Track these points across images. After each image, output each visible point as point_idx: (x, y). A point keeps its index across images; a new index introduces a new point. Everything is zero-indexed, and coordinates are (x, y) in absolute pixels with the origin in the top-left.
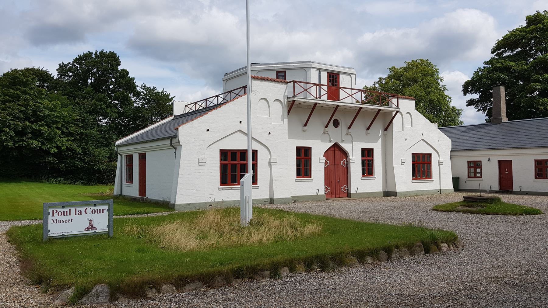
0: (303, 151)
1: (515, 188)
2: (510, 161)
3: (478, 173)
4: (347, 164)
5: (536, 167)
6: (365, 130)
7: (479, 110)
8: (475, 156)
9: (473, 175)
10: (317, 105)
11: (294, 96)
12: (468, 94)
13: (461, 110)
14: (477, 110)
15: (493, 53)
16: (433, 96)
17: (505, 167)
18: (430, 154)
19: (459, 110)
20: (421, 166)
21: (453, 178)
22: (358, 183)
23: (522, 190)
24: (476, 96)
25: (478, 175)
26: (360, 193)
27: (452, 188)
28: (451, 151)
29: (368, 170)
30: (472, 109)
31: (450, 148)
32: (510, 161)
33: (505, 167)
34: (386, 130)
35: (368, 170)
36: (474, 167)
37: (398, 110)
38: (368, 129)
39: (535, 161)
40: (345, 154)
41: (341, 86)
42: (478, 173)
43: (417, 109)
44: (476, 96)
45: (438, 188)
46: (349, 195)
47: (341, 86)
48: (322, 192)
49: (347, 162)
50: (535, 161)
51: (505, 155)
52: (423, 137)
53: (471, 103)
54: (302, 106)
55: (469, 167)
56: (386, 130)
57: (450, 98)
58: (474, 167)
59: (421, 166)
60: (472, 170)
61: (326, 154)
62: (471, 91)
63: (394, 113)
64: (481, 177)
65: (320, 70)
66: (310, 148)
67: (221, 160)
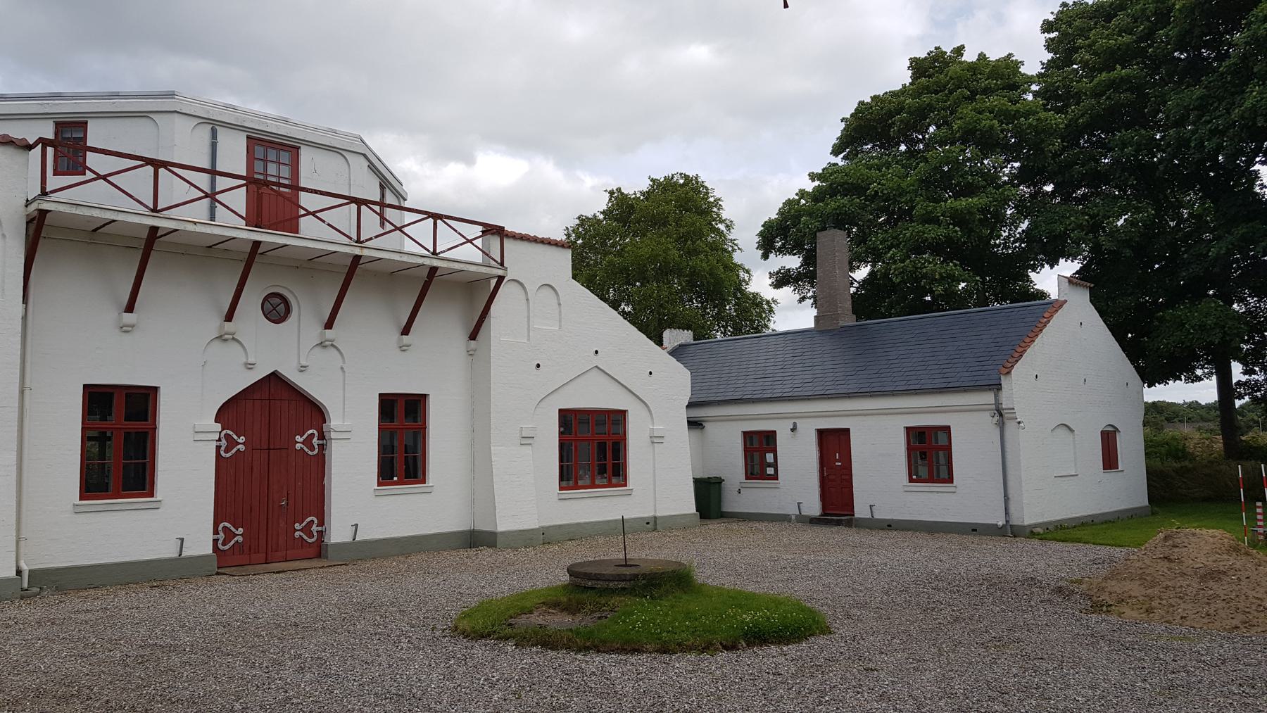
0: (399, 410)
1: (861, 511)
2: (846, 432)
3: (770, 465)
4: (322, 447)
5: (910, 449)
6: (396, 335)
7: (802, 299)
8: (761, 418)
9: (757, 469)
10: (48, 215)
11: (44, 193)
12: (772, 256)
13: (774, 301)
14: (798, 297)
15: (836, 152)
16: (700, 262)
17: (834, 445)
18: (623, 413)
19: (768, 302)
20: (592, 446)
21: (698, 482)
22: (357, 503)
23: (876, 516)
24: (793, 262)
25: (770, 471)
26: (191, 558)
27: (693, 510)
28: (690, 405)
29: (402, 459)
30: (786, 294)
31: (686, 396)
32: (846, 432)
33: (834, 445)
34: (473, 336)
35: (402, 459)
36: (760, 448)
37: (500, 272)
38: (406, 331)
39: (909, 430)
40: (315, 413)
41: (302, 185)
42: (770, 465)
43: (574, 277)
44: (793, 262)
45: (651, 514)
46: (318, 550)
47: (568, 254)
48: (201, 543)
49: (322, 437)
50: (909, 430)
51: (833, 414)
52: (597, 361)
53: (782, 279)
54: (96, 237)
55: (748, 451)
56: (473, 336)
57: (748, 271)
58: (760, 448)
59: (592, 446)
60: (756, 456)
61: (229, 413)
62: (781, 251)
63: (494, 282)
64: (775, 477)
65: (214, 126)
66: (424, 397)
67: (561, 433)
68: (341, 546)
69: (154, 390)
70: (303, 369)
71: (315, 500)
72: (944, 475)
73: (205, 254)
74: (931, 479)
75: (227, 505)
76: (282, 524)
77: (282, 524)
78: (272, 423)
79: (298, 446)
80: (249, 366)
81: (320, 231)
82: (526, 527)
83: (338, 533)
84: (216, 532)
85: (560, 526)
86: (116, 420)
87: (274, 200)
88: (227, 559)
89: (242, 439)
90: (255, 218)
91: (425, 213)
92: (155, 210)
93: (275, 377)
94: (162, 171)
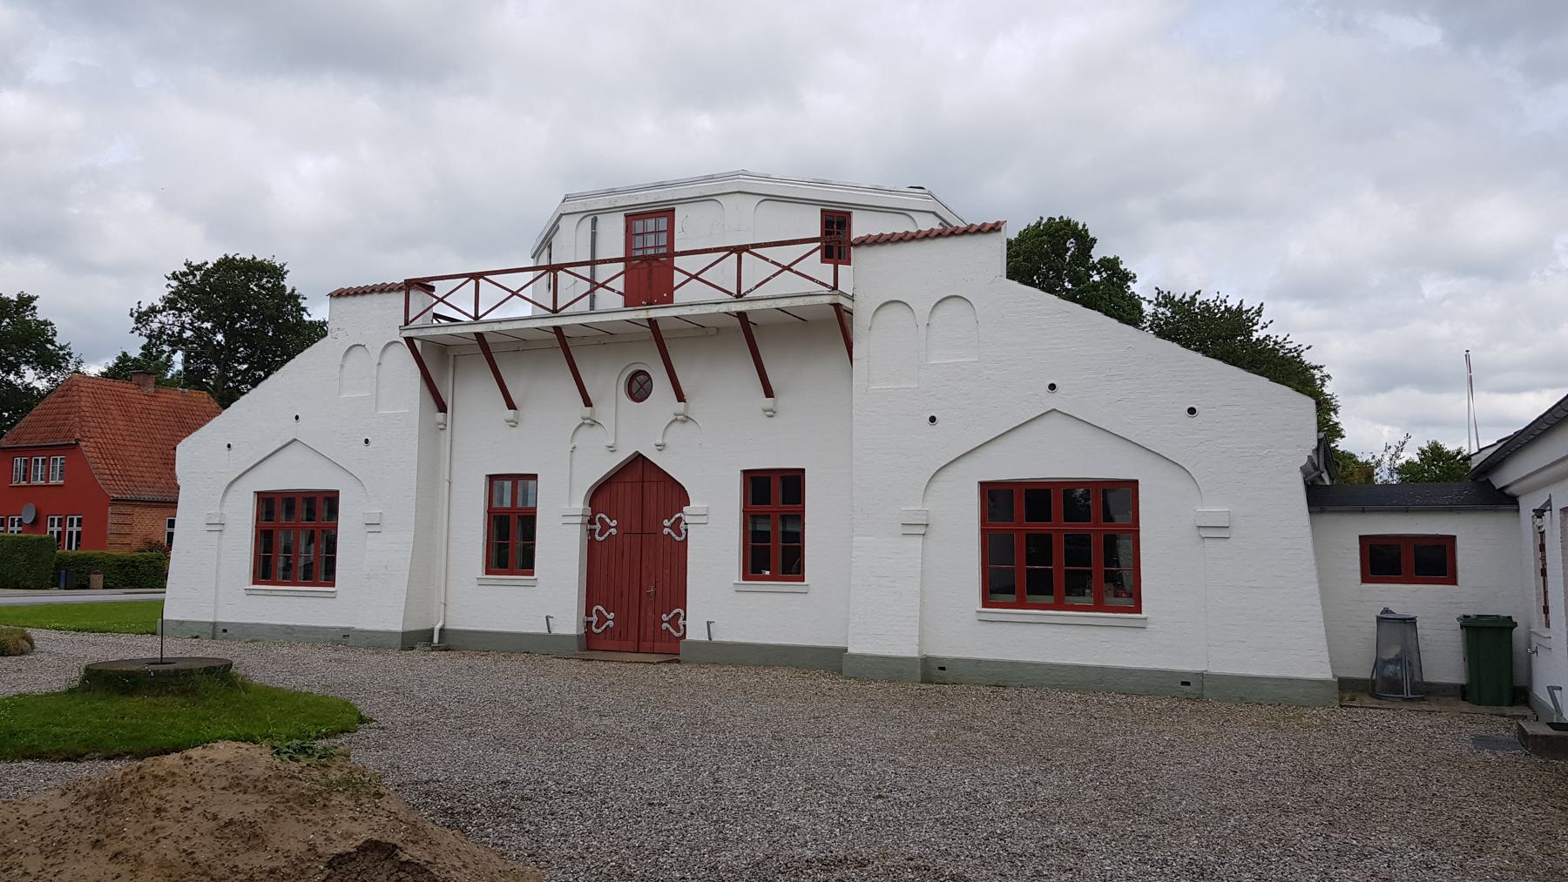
22: (718, 597)
40: (676, 495)
48: (569, 623)
61: (601, 495)
65: (594, 216)
68: (697, 644)
69: (983, 485)
70: (661, 447)
71: (677, 595)
72: (516, 556)
73: (606, 339)
74: (265, 538)
75: (597, 587)
76: (650, 613)
77: (650, 613)
78: (637, 503)
79: (666, 531)
80: (612, 449)
81: (693, 297)
82: (894, 653)
83: (695, 631)
84: (589, 614)
85: (979, 661)
86: (1021, 526)
87: (649, 273)
88: (590, 643)
89: (614, 523)
90: (631, 300)
91: (726, 249)
92: (739, 295)
93: (638, 460)
94: (745, 255)
